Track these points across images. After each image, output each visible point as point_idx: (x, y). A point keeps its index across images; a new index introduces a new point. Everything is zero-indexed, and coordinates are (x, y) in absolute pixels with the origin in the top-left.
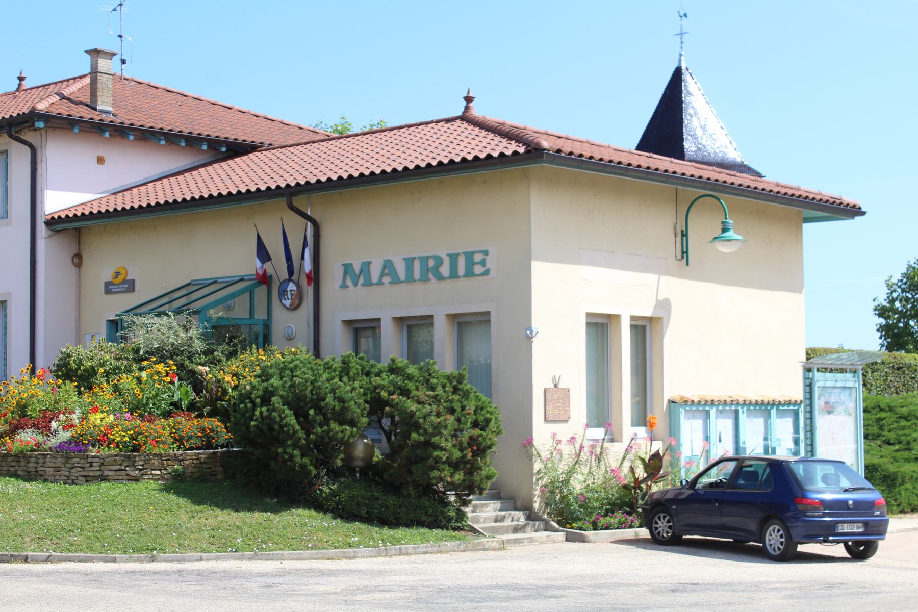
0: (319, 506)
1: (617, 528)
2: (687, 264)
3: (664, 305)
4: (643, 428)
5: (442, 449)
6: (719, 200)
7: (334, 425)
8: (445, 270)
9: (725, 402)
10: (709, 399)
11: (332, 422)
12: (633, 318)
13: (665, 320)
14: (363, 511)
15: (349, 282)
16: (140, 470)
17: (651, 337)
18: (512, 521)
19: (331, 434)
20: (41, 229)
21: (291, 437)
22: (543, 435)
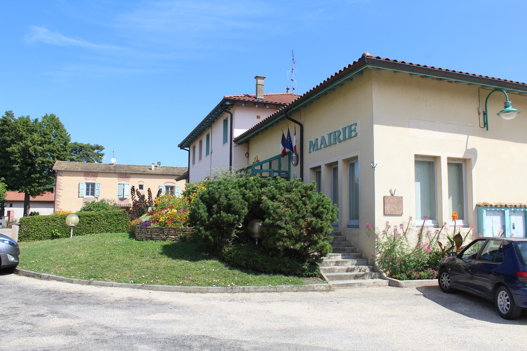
0: (222, 260)
1: (428, 279)
2: (487, 130)
3: (474, 152)
4: (461, 221)
5: (283, 228)
6: (502, 91)
7: (223, 214)
8: (341, 137)
9: (515, 206)
10: (504, 204)
11: (222, 212)
12: (449, 159)
13: (473, 160)
14: (244, 263)
15: (312, 150)
16: (166, 235)
17: (466, 170)
18: (360, 271)
19: (221, 218)
20: (233, 142)
21: (200, 220)
22: (380, 222)
